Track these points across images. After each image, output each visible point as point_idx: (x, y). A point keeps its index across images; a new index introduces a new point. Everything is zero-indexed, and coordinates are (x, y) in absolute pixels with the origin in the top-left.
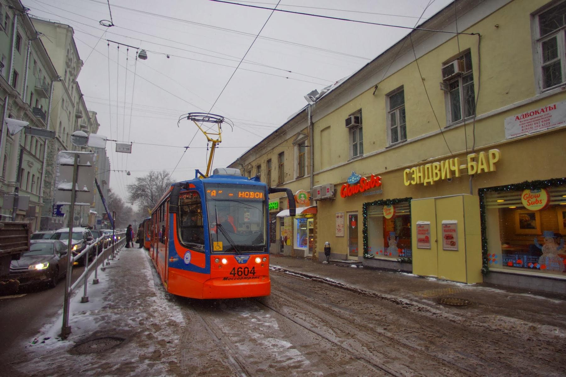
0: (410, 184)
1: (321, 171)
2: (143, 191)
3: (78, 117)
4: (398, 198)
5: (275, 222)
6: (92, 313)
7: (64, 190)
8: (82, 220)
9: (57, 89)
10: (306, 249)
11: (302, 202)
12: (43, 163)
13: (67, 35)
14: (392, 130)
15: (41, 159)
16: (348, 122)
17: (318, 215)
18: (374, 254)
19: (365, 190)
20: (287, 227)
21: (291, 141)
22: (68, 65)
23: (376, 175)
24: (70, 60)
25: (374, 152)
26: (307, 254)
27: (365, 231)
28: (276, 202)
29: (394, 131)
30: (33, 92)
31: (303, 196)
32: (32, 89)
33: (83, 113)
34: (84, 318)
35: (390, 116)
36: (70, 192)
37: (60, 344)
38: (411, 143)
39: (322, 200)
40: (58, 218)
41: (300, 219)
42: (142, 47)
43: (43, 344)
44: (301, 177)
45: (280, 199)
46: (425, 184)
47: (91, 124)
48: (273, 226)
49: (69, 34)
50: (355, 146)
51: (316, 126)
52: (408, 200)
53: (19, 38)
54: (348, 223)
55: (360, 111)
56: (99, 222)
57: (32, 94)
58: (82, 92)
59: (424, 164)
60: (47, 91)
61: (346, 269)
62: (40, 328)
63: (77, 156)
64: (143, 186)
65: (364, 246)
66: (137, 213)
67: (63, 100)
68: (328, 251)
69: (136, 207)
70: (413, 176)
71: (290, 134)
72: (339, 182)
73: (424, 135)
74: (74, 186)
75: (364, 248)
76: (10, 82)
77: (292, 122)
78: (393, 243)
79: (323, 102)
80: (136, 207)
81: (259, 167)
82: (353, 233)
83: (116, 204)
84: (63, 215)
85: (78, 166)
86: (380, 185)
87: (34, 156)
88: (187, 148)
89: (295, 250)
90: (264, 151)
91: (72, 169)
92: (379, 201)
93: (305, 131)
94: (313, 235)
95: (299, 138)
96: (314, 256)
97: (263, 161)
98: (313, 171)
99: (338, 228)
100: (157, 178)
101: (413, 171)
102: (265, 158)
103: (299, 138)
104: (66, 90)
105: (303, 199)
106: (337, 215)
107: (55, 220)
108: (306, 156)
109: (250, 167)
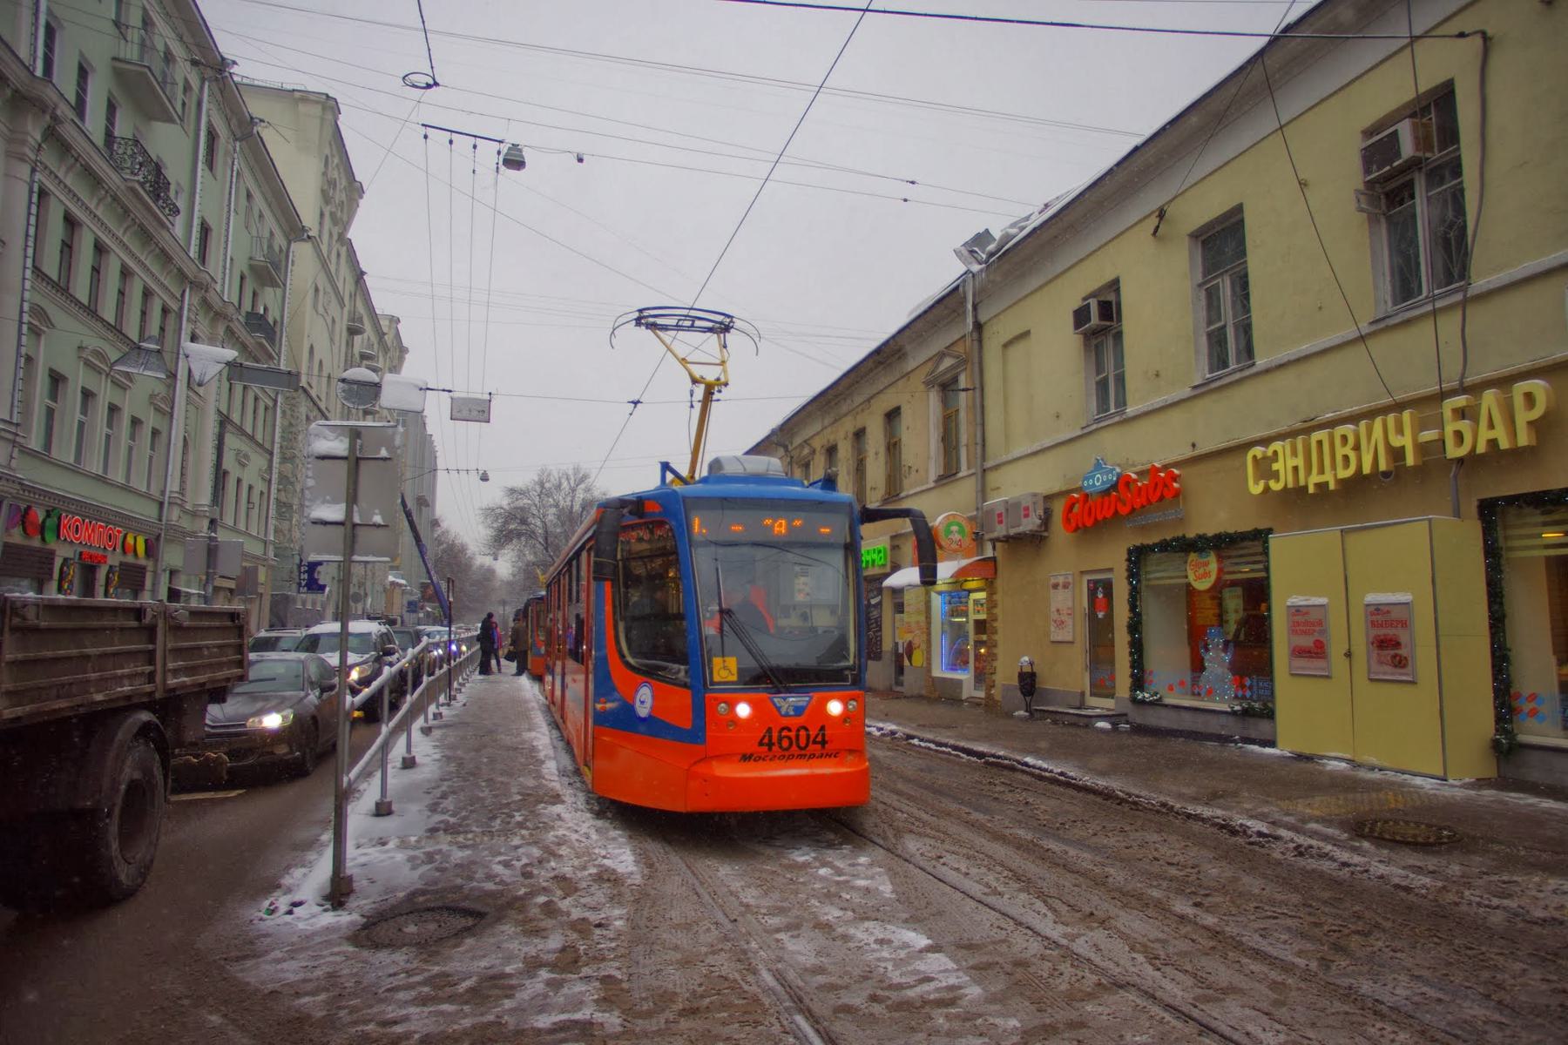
0: (1267, 489)
1: (1005, 458)
2: (524, 522)
3: (353, 331)
4: (1231, 531)
5: (880, 603)
6: (404, 845)
7: (325, 523)
8: (369, 601)
9: (303, 264)
10: (965, 676)
11: (954, 546)
12: (271, 454)
13: (322, 119)
14: (1209, 335)
15: (268, 446)
16: (1081, 316)
17: (999, 582)
18: (1163, 691)
19: (1133, 510)
20: (911, 616)
21: (917, 380)
22: (326, 198)
23: (1165, 467)
24: (332, 183)
25: (1158, 401)
26: (969, 690)
27: (1135, 627)
28: (881, 547)
29: (1217, 341)
30: (246, 273)
31: (954, 528)
32: (242, 265)
33: (366, 320)
34: (383, 856)
35: (1203, 294)
36: (341, 528)
37: (329, 918)
38: (1267, 371)
39: (1007, 539)
40: (310, 597)
41: (949, 593)
42: (511, 139)
43: (288, 918)
44: (948, 475)
45: (893, 538)
46: (1311, 490)
47: (386, 350)
48: (875, 613)
49: (329, 117)
50: (1102, 386)
51: (987, 333)
52: (1260, 536)
53: (212, 137)
54: (1086, 604)
55: (1115, 285)
56: (413, 607)
57: (242, 278)
58: (364, 267)
59: (1307, 431)
60: (276, 267)
61: (1081, 732)
62: (282, 877)
63: (355, 434)
64: (522, 509)
65: (1132, 667)
66: (509, 584)
67: (317, 290)
68: (1028, 682)
69: (504, 566)
70: (1275, 467)
71: (917, 358)
72: (1056, 486)
73: (1306, 348)
74: (349, 512)
75: (1132, 675)
76: (193, 251)
77: (919, 324)
78: (1218, 662)
79: (1009, 262)
80: (504, 566)
81: (831, 451)
82: (1100, 632)
83: (453, 559)
84: (322, 588)
85: (358, 459)
86: (1177, 494)
87: (252, 438)
88: (636, 403)
89: (934, 679)
90: (844, 408)
91: (342, 469)
92: (1174, 540)
93: (960, 349)
94: (984, 637)
95: (942, 368)
96: (989, 696)
97: (842, 434)
98: (984, 458)
99: (1055, 616)
100: (558, 487)
101: (1275, 453)
102: (849, 426)
103: (942, 368)
104: (324, 265)
105: (957, 537)
106: (1053, 581)
107: (304, 603)
108: (962, 414)
109: (806, 451)
